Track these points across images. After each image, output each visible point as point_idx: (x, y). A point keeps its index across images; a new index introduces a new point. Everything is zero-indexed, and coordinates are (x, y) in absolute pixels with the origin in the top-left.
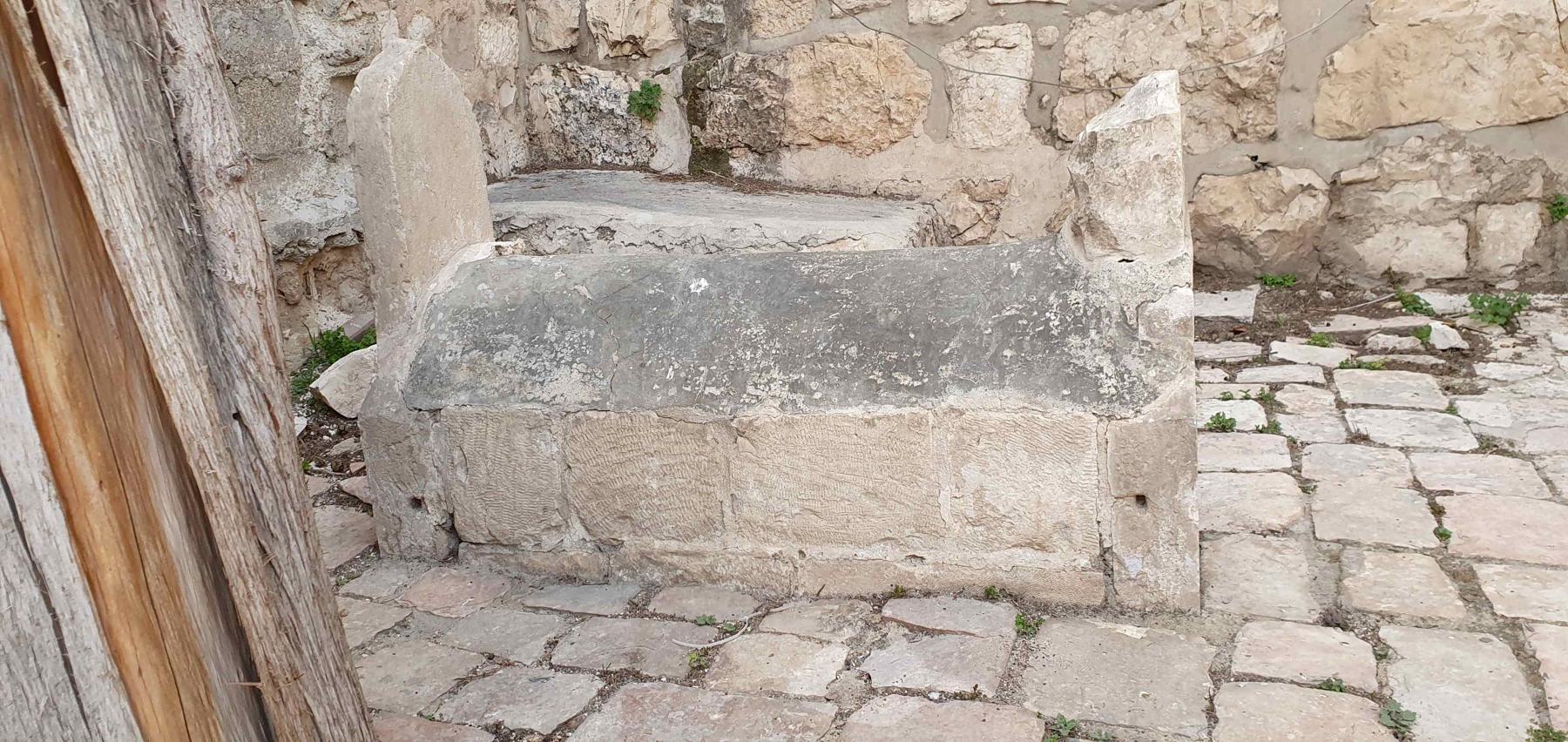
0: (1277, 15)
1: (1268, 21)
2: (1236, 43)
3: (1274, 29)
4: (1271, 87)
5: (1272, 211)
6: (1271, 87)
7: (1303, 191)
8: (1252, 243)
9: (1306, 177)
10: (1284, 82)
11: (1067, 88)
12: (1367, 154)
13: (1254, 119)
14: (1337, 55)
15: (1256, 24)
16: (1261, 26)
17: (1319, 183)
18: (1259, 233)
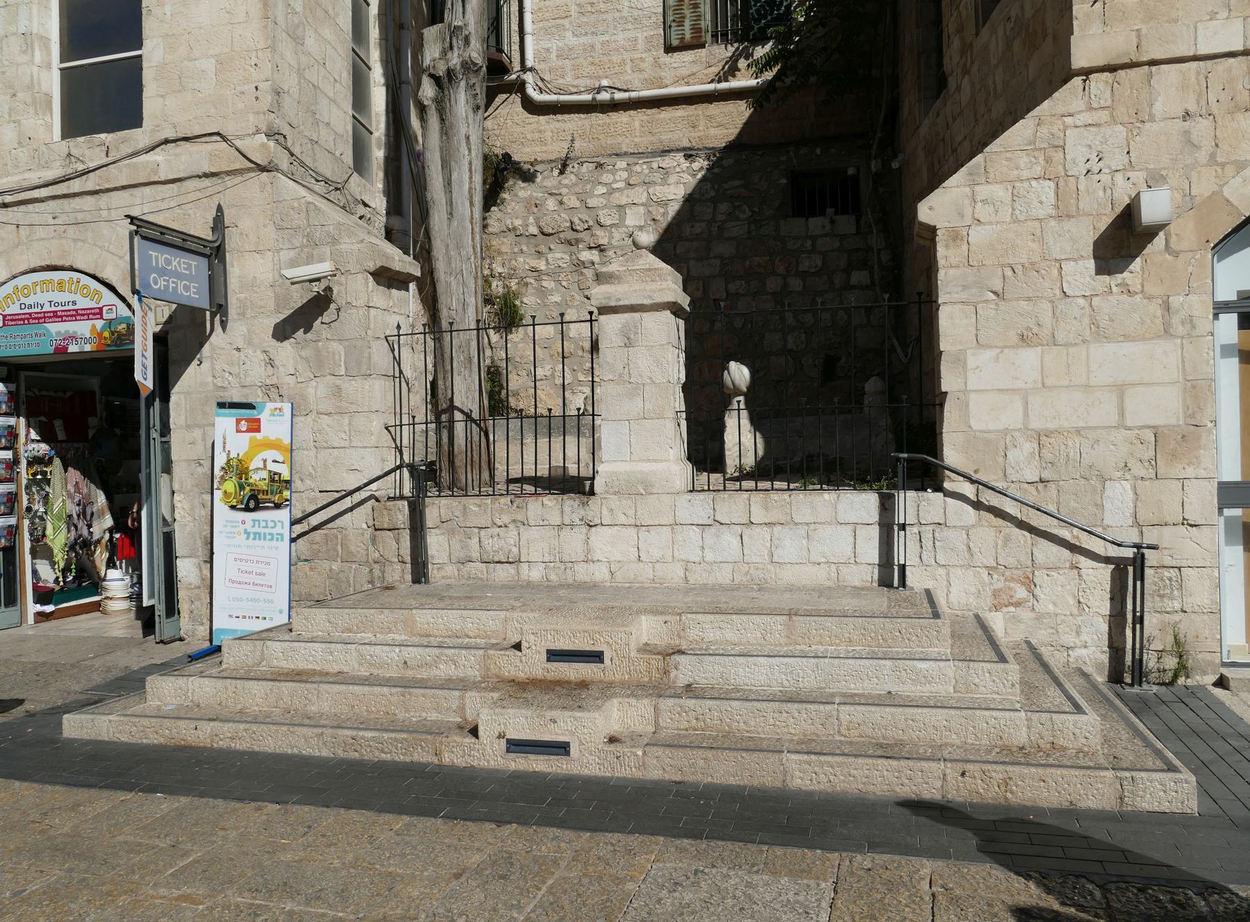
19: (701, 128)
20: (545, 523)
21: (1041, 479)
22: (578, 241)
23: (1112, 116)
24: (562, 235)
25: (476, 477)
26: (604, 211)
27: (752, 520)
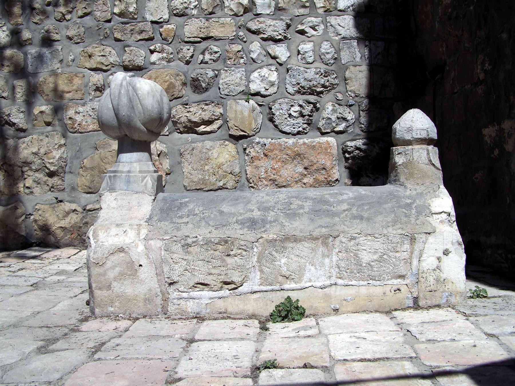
0: (65, 144)
1: (61, 146)
2: (49, 153)
3: (63, 149)
4: (62, 171)
5: (298, 117)
6: (62, 171)
7: (73, 212)
8: (53, 232)
9: (74, 206)
10: (67, 169)
11: (29, 169)
12: (96, 199)
13: (57, 183)
14: (85, 161)
15: (56, 147)
16: (58, 147)
17: (79, 209)
18: (56, 228)
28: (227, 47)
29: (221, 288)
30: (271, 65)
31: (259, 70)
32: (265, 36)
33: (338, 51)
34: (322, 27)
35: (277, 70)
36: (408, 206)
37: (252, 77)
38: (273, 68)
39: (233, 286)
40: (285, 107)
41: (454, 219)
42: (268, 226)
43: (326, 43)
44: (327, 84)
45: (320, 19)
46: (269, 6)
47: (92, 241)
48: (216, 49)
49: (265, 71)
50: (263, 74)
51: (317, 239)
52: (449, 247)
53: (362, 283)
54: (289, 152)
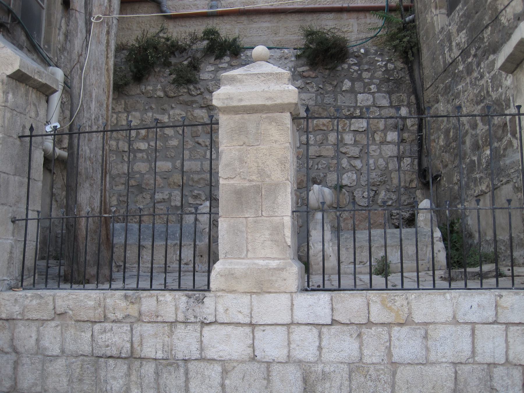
19: (280, 35)
20: (159, 319)
21: (63, 351)
22: (193, 102)
23: (303, 144)
24: (181, 98)
25: (173, 256)
26: (213, 82)
27: (372, 319)
28: (330, 161)
29: (359, 264)
30: (352, 170)
31: (347, 173)
32: (350, 156)
33: (387, 164)
34: (379, 151)
35: (356, 173)
36: (425, 235)
37: (343, 177)
38: (354, 172)
39: (363, 263)
40: (360, 193)
41: (442, 240)
42: (375, 242)
43: (381, 159)
44: (382, 181)
45: (377, 147)
46: (351, 140)
47: (312, 247)
48: (324, 162)
49: (350, 174)
50: (349, 176)
51: (393, 246)
52: (440, 249)
53: (409, 262)
54: (363, 216)
